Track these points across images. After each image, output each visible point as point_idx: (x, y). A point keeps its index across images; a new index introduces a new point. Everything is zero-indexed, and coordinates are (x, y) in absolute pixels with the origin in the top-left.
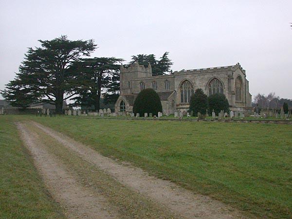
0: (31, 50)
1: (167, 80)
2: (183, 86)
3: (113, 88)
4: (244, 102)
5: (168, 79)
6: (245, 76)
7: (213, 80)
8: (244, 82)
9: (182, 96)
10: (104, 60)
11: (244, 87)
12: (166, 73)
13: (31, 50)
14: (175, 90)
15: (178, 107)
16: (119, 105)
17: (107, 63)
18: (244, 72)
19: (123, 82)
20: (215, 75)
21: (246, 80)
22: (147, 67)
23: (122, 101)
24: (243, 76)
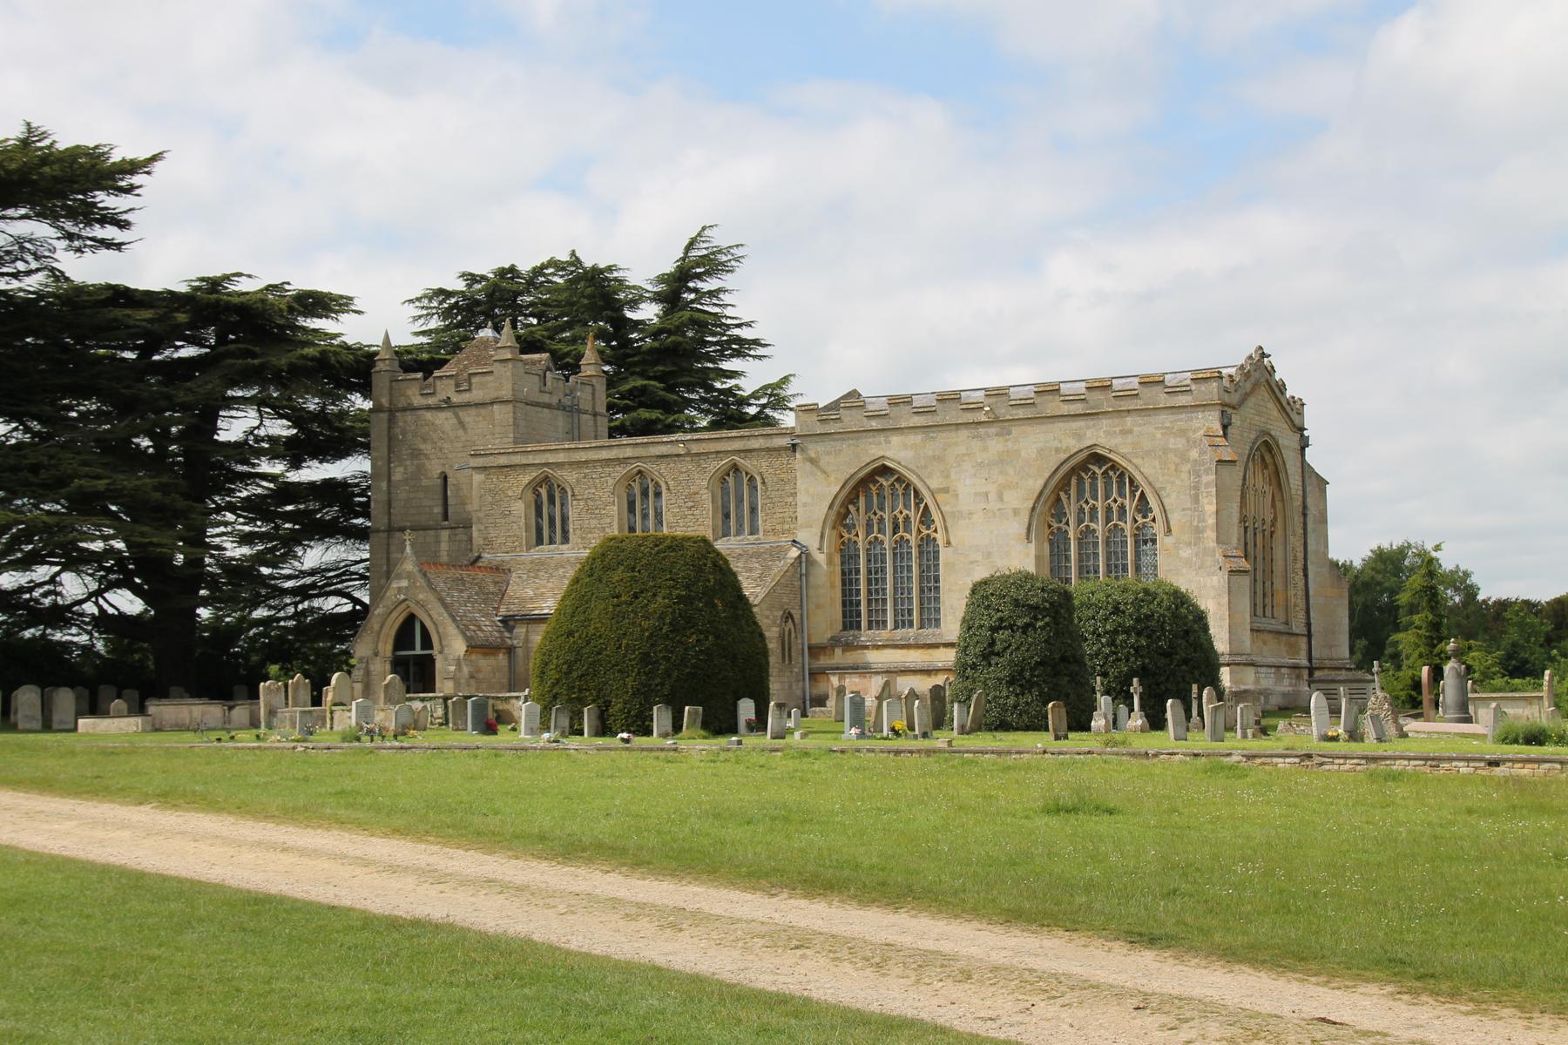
0: (1467, 575)
1: (736, 468)
2: (859, 517)
3: (288, 517)
4: (1298, 626)
5: (745, 463)
6: (1304, 444)
7: (1083, 467)
8: (1295, 481)
9: (848, 580)
10: (209, 306)
11: (1298, 519)
12: (100, 646)
13: (1467, 575)
14: (802, 537)
15: (823, 661)
16: (387, 648)
17: (256, 335)
18: (1291, 411)
19: (398, 475)
20: (1100, 435)
21: (1305, 468)
22: (575, 368)
23: (411, 618)
24: (1287, 441)
